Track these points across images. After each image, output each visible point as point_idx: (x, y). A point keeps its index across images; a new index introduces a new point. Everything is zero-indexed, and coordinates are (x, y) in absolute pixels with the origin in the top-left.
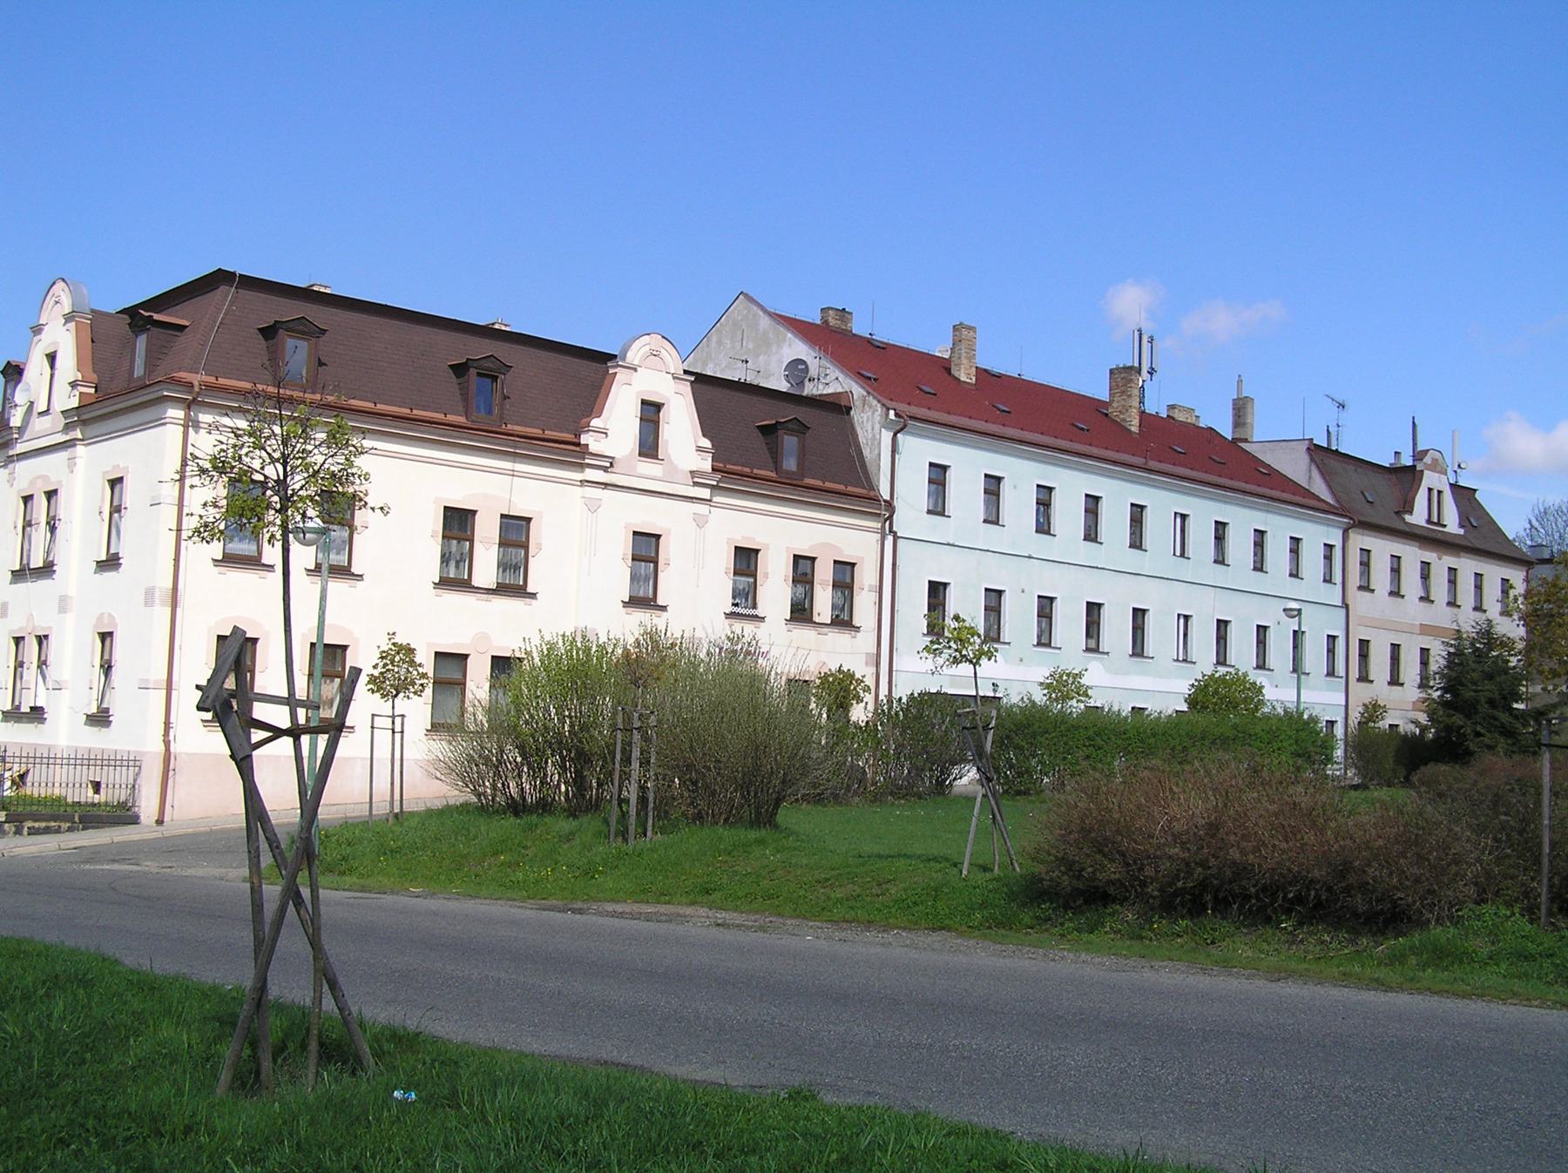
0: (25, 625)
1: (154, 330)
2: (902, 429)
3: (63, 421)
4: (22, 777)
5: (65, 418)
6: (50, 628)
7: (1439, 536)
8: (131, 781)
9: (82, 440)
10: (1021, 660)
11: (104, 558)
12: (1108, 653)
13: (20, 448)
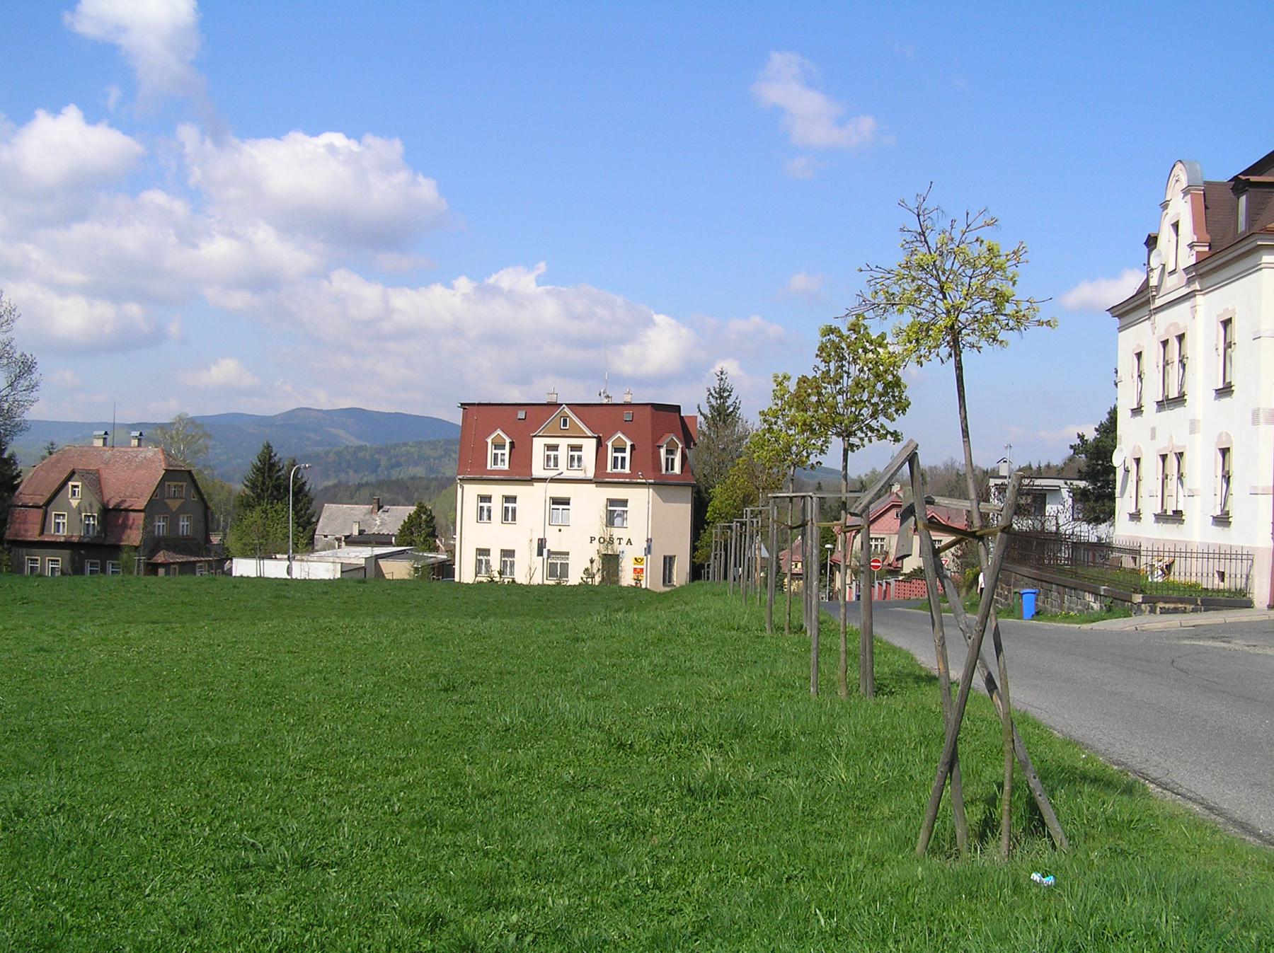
0: (1167, 445)
1: (1252, 190)
3: (1185, 278)
4: (1169, 567)
5: (1187, 274)
6: (1185, 446)
8: (1245, 571)
9: (1201, 291)
11: (1221, 386)
13: (1158, 303)
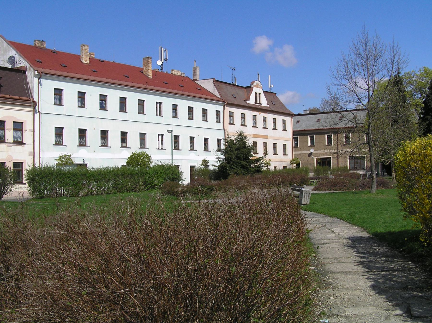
2: (40, 77)
7: (259, 107)
10: (95, 151)
12: (148, 148)
